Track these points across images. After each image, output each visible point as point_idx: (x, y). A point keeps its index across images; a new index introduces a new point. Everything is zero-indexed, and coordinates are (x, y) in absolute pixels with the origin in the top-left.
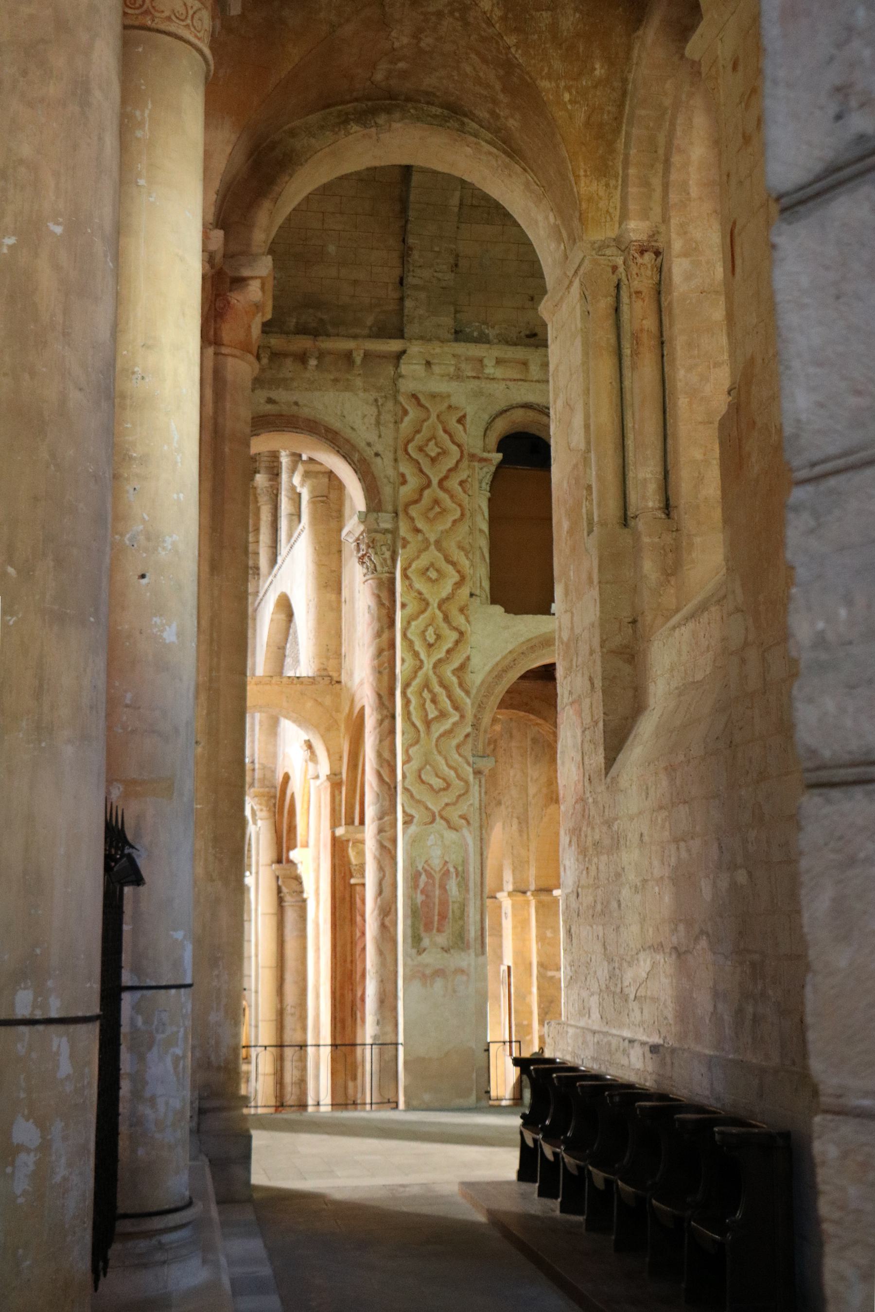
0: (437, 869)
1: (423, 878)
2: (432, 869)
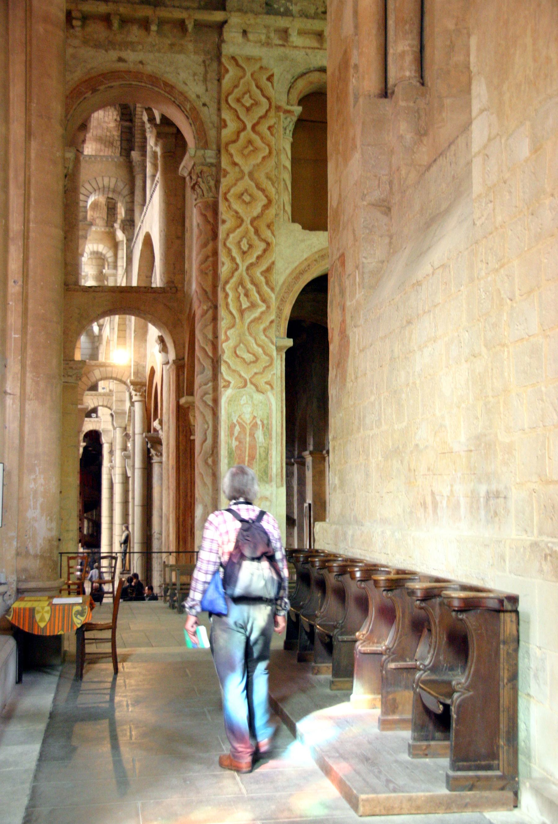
0: (248, 422)
1: (237, 428)
2: (244, 422)
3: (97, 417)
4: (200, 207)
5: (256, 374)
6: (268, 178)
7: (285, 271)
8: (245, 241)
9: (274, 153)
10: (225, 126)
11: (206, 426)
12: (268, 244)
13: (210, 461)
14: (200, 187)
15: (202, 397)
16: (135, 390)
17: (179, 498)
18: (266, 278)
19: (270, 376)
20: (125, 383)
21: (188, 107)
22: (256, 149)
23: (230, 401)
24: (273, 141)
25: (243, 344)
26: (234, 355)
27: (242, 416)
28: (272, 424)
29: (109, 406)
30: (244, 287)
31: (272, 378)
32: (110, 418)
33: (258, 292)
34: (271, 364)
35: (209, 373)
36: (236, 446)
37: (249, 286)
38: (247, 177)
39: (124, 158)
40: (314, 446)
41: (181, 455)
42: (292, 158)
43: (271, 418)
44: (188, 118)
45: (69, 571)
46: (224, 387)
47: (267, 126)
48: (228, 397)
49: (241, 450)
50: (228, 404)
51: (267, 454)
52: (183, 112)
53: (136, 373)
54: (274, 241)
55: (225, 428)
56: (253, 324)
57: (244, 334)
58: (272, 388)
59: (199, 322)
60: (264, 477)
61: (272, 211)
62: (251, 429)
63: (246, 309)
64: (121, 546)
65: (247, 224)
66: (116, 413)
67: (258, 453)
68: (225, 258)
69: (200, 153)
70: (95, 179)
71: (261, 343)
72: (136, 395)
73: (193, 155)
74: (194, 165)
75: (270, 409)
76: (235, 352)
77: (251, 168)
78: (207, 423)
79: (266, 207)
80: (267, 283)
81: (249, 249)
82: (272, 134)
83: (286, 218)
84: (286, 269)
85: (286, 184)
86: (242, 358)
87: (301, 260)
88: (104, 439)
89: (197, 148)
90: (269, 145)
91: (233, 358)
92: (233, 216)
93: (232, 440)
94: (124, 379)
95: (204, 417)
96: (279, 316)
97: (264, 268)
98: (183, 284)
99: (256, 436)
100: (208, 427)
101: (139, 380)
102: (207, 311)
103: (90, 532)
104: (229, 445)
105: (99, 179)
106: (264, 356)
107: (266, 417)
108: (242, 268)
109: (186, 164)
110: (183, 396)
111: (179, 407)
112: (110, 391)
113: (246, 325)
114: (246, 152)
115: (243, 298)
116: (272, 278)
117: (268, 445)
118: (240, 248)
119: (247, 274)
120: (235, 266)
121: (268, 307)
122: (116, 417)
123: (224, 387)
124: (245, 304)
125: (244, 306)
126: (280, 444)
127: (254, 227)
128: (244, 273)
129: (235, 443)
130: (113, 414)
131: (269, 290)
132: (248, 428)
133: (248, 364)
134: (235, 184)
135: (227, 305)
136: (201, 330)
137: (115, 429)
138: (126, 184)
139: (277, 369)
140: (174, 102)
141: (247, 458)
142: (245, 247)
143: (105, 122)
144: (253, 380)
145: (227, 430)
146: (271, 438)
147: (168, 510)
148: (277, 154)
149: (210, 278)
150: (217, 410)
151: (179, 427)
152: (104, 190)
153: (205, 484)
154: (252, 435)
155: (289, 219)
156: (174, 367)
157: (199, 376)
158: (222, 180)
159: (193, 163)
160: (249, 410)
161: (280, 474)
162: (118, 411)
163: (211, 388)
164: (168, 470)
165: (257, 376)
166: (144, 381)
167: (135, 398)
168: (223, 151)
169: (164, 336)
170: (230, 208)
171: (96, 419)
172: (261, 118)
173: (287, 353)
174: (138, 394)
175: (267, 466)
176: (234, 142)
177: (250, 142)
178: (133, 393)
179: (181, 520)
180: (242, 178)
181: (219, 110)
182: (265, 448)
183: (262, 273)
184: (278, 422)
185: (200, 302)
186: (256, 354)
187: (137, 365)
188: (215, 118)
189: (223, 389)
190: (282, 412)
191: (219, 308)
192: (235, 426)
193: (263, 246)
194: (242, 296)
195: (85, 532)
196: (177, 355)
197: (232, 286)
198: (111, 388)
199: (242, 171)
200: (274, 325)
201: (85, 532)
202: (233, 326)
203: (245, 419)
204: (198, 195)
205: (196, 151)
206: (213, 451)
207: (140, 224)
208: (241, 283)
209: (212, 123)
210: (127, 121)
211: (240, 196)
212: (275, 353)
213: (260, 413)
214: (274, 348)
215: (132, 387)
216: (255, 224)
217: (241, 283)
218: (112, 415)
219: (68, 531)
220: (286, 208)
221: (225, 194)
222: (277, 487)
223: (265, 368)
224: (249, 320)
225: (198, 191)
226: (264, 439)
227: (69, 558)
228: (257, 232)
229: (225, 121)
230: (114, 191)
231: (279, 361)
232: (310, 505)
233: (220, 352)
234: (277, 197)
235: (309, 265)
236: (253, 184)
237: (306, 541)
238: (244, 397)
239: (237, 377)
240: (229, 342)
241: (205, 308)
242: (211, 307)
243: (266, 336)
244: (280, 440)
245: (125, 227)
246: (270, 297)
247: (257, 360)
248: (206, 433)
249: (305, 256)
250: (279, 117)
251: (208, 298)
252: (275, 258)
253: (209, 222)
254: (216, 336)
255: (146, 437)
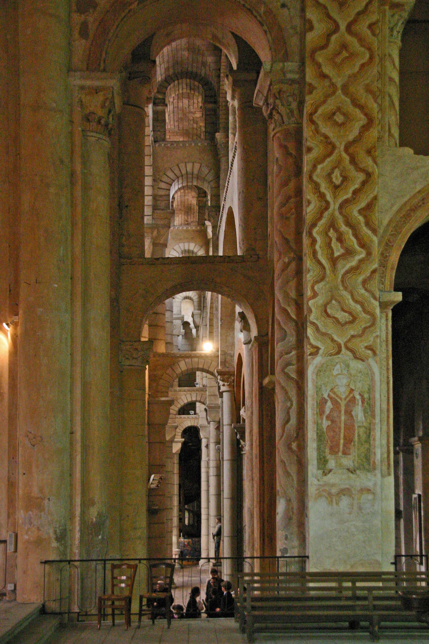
0: (343, 397)
1: (329, 404)
2: (337, 396)
3: (195, 414)
4: (278, 137)
5: (353, 336)
6: (368, 90)
7: (391, 208)
8: (337, 172)
9: (377, 59)
10: (311, 28)
11: (289, 404)
12: (369, 175)
13: (294, 446)
14: (278, 113)
15: (283, 370)
16: (223, 381)
17: (264, 491)
18: (365, 217)
19: (372, 339)
20: (212, 374)
21: (262, 10)
22: (352, 56)
23: (319, 371)
24: (374, 42)
25: (336, 300)
26: (324, 314)
27: (335, 390)
28: (375, 398)
29: (202, 401)
30: (336, 230)
31: (374, 341)
32: (205, 413)
33: (356, 236)
34: (373, 324)
35: (292, 339)
36: (328, 426)
37: (344, 228)
38: (339, 85)
39: (208, 141)
40: (424, 429)
41: (265, 442)
42: (400, 70)
43: (374, 391)
44: (262, 25)
45: (113, 582)
46: (311, 354)
47: (367, 24)
48: (316, 367)
49: (334, 431)
50: (317, 375)
51: (369, 436)
52: (256, 17)
53: (224, 363)
54: (377, 170)
55: (313, 405)
56: (349, 275)
57: (338, 289)
58: (375, 353)
59: (278, 279)
60: (365, 464)
61: (374, 133)
62: (347, 405)
63: (339, 257)
64: (214, 538)
65: (340, 152)
66: (210, 407)
67: (356, 435)
68: (311, 194)
69: (279, 66)
70: (178, 165)
71: (359, 299)
72: (224, 385)
73: (268, 70)
74: (271, 84)
75: (373, 380)
76: (326, 311)
77: (346, 79)
78: (291, 400)
79: (366, 128)
80: (367, 224)
81: (342, 182)
82: (374, 34)
83: (392, 143)
84: (392, 205)
85: (392, 102)
86: (334, 317)
87: (412, 194)
88: (202, 435)
89: (273, 62)
90: (369, 49)
91: (323, 319)
92: (321, 142)
93: (322, 419)
94: (211, 370)
95: (287, 393)
96: (383, 264)
97: (363, 204)
98: (265, 250)
99: (353, 413)
100: (292, 405)
101: (227, 370)
102: (289, 263)
103: (191, 522)
104: (318, 425)
105: (182, 166)
106: (364, 315)
107: (367, 389)
108: (334, 206)
109: (260, 88)
110: (266, 376)
111: (261, 388)
112: (204, 386)
113: (340, 276)
114: (338, 60)
115: (335, 244)
116: (374, 218)
117: (370, 424)
118: (331, 182)
119: (341, 213)
120: (324, 204)
121: (369, 254)
122: (209, 411)
123: (311, 354)
124: (338, 251)
125: (336, 254)
126: (385, 423)
127: (349, 154)
128: (337, 213)
129: (326, 423)
130: (207, 408)
131: (369, 232)
132: (343, 404)
133: (343, 325)
134: (324, 102)
135: (315, 253)
136: (281, 288)
137: (209, 423)
138: (211, 170)
139: (381, 331)
140: (244, 5)
141: (342, 441)
142: (337, 179)
143: (190, 112)
144: (349, 345)
145: (315, 406)
146: (373, 416)
147: (252, 504)
148: (381, 60)
149: (292, 223)
150: (303, 383)
151: (262, 411)
152: (187, 178)
153: (287, 474)
154: (349, 413)
155: (396, 144)
156: (256, 345)
157: (280, 344)
158: (307, 98)
159: (269, 83)
160: (345, 381)
161: (386, 460)
162: (211, 405)
163: (295, 357)
164: (251, 460)
165: (354, 340)
166: (232, 370)
167: (223, 389)
168: (308, 62)
169: (244, 312)
170: (318, 132)
171: (194, 416)
172: (359, 14)
173: (394, 311)
174: (226, 384)
175: (368, 450)
176: (324, 47)
177: (344, 46)
178: (221, 383)
179: (266, 515)
180: (334, 93)
181: (303, 10)
182: (366, 428)
183: (360, 212)
184: (382, 396)
185: (280, 254)
186: (354, 313)
187: (224, 353)
188: (297, 22)
189: (309, 357)
190: (388, 383)
191: (304, 258)
192: (326, 401)
193: (361, 177)
194: (334, 240)
195: (187, 522)
196: (259, 331)
197: (321, 229)
198: (204, 383)
199: (333, 85)
200: (377, 276)
201: (187, 522)
202: (323, 279)
203: (338, 393)
204: (275, 122)
205: (272, 64)
206: (298, 435)
207: (223, 203)
208: (332, 225)
209: (294, 28)
210: (211, 102)
211: (330, 116)
212: (378, 311)
213: (359, 385)
214: (377, 303)
215: (219, 377)
216: (351, 150)
217: (332, 225)
218: (206, 410)
219: (135, 529)
220: (393, 131)
221: (311, 115)
222: (383, 476)
223: (365, 329)
224: (343, 271)
225: (276, 118)
226: (365, 417)
227: (114, 567)
228: (353, 161)
229: (310, 22)
230: (198, 178)
231: (383, 321)
232: (419, 496)
233: (305, 312)
234: (380, 116)
235: (423, 199)
236: (348, 100)
237: (416, 536)
238: (338, 366)
239: (329, 341)
240: (317, 299)
241: (286, 260)
242: (294, 258)
243: (366, 290)
244: (386, 418)
245: (210, 213)
246: (372, 241)
247: (354, 319)
248: (288, 413)
249: (418, 188)
250: (384, 12)
251: (290, 247)
252: (378, 192)
253: (291, 155)
254: (300, 293)
255: (235, 428)
